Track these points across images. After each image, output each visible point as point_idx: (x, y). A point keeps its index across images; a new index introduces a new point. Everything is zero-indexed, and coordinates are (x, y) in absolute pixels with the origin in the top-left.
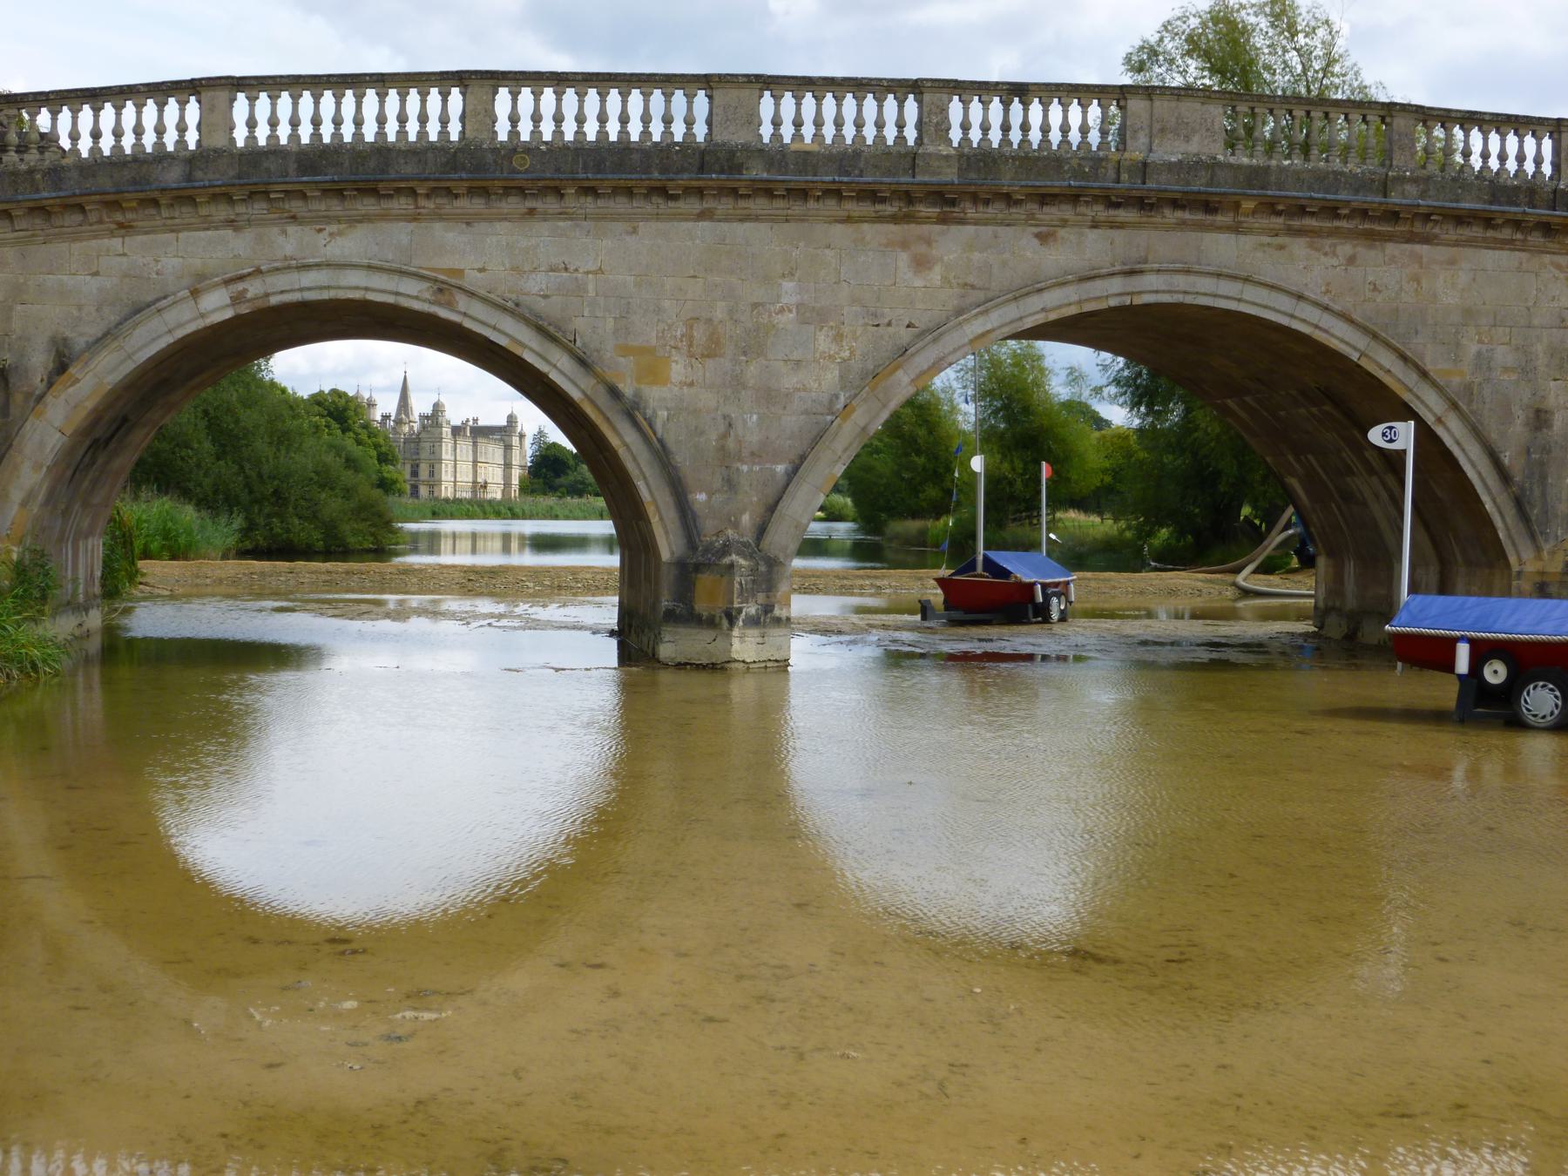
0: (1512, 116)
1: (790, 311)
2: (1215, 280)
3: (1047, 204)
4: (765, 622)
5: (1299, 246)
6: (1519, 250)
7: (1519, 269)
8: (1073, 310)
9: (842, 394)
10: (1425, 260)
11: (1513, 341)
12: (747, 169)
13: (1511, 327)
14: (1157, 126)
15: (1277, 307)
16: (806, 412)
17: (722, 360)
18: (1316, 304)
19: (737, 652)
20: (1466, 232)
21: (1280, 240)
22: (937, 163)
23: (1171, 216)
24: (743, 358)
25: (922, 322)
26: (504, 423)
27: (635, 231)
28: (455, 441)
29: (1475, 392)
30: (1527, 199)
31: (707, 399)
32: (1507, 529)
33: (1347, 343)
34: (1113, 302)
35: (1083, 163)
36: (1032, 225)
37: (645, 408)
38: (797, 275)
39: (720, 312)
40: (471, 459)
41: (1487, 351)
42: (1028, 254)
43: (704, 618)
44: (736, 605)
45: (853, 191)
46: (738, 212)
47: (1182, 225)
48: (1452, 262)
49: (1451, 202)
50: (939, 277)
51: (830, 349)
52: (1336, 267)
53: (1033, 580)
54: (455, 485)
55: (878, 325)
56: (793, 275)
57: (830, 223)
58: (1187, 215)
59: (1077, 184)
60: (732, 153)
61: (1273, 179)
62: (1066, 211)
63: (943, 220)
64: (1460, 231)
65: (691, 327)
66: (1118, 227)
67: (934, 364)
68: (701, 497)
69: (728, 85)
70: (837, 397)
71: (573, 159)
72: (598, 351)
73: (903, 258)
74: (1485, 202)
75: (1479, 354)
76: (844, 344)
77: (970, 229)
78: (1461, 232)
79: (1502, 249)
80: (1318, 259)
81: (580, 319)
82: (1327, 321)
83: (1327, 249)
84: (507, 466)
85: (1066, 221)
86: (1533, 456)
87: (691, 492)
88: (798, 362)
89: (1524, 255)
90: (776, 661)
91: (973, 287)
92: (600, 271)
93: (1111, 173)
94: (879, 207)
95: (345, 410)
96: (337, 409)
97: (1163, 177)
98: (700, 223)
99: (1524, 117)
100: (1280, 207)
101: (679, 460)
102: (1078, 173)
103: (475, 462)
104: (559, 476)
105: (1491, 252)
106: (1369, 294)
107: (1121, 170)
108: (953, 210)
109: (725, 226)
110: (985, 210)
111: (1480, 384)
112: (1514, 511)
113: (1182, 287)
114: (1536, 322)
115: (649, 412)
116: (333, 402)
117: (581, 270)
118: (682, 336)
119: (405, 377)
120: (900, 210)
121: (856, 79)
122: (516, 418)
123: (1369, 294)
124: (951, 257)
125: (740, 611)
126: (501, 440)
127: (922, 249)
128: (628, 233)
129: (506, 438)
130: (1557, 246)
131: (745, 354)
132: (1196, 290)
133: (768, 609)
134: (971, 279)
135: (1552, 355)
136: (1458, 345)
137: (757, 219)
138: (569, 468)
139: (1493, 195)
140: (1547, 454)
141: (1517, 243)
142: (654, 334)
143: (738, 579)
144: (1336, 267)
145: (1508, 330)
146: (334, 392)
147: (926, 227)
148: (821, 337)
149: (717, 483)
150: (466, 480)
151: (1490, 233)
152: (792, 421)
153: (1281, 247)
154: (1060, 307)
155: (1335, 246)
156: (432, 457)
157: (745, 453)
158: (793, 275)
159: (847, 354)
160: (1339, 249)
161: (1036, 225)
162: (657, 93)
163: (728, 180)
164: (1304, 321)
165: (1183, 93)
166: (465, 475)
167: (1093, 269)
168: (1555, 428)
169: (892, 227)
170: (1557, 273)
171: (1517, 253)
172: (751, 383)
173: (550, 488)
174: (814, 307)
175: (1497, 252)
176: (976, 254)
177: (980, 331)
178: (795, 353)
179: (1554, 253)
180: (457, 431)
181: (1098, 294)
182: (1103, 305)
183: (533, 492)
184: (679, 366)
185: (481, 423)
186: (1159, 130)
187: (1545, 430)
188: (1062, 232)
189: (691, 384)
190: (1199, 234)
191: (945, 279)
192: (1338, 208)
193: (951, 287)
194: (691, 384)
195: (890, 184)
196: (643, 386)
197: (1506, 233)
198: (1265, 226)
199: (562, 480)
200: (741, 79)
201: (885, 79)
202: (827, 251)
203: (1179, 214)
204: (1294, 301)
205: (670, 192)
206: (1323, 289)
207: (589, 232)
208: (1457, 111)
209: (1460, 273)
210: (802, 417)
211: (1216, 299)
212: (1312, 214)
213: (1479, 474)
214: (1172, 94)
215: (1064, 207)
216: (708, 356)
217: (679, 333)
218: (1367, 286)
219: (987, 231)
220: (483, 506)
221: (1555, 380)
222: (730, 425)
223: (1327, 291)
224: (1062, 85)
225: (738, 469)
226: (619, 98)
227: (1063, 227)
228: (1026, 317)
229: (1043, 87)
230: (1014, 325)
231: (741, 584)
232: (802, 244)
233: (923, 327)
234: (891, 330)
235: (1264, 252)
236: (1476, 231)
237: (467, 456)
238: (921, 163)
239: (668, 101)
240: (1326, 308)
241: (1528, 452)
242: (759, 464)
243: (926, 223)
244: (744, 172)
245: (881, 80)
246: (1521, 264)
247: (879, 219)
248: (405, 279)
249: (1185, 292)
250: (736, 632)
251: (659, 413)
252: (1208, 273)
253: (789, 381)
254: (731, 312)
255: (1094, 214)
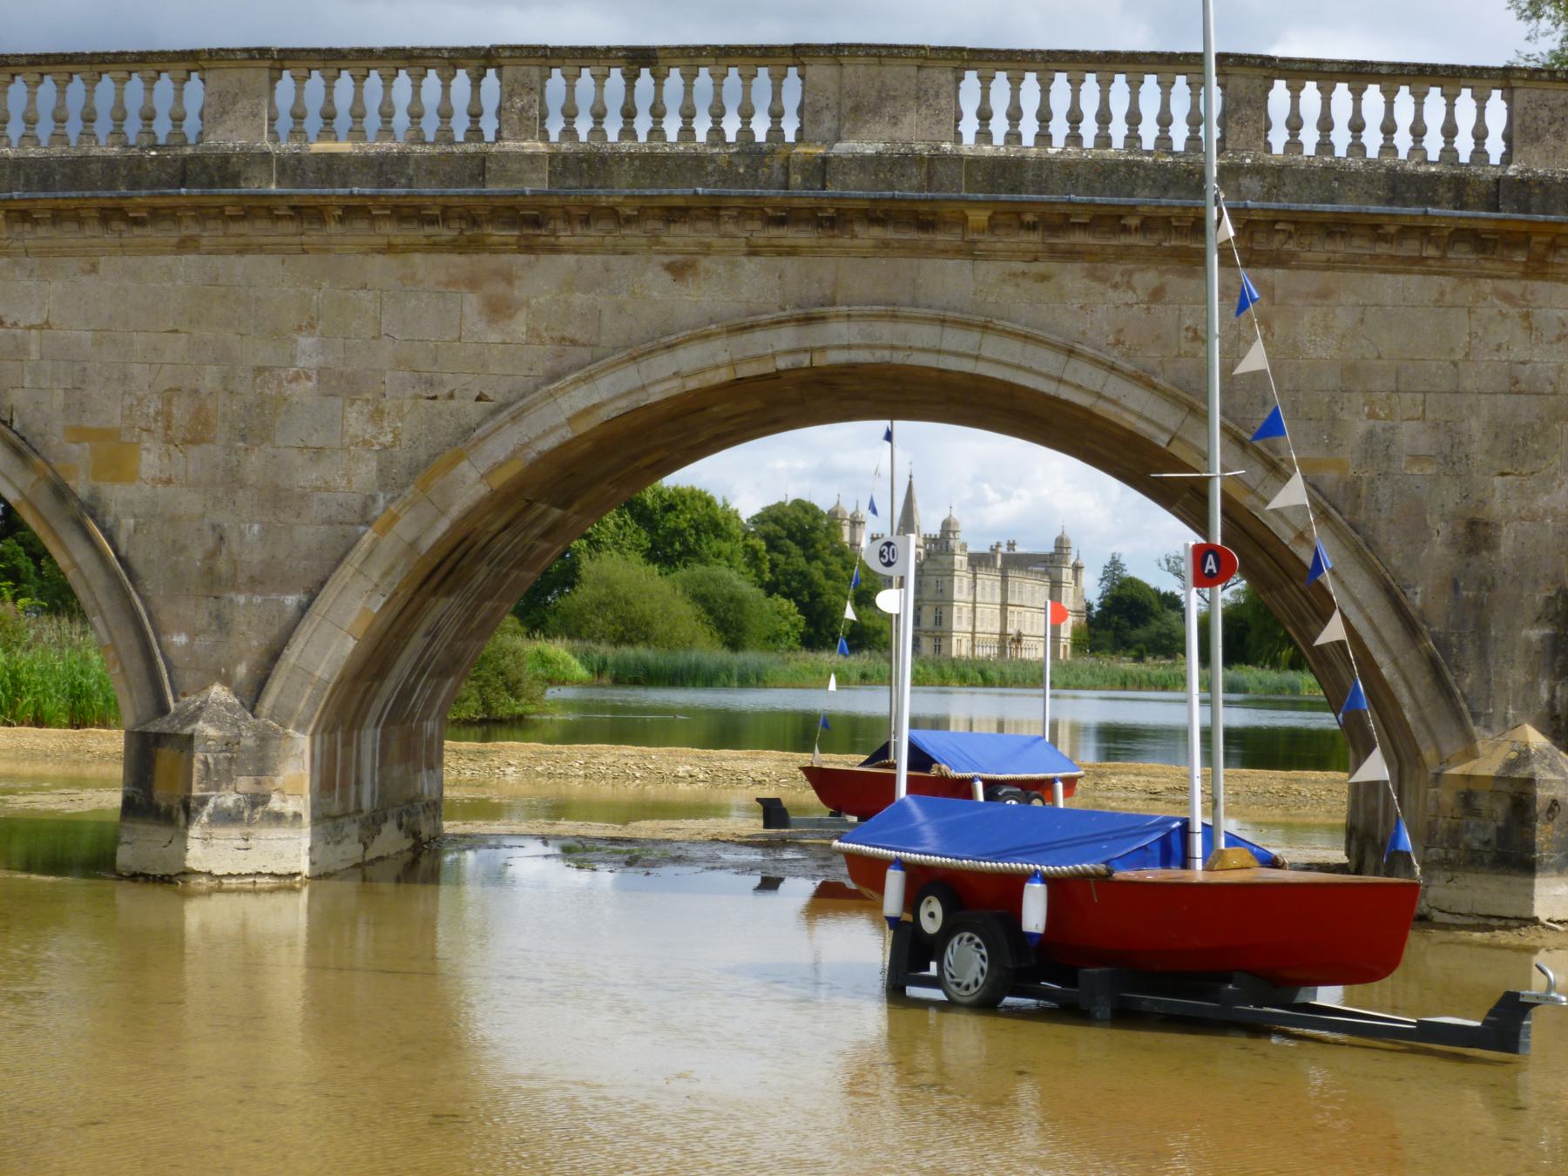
0: (1425, 66)
1: (309, 378)
2: (938, 328)
3: (675, 222)
4: (251, 817)
5: (1072, 277)
6: (1439, 274)
7: (1439, 302)
8: (723, 376)
9: (382, 495)
10: (1278, 291)
11: (1429, 415)
12: (246, 179)
13: (1424, 393)
14: (849, 103)
15: (1035, 367)
16: (329, 522)
17: (211, 447)
18: (1096, 362)
19: (196, 859)
20: (1340, 248)
21: (1040, 267)
22: (516, 167)
23: (869, 235)
24: (241, 444)
25: (497, 396)
26: (987, 550)
27: (94, 269)
28: (975, 575)
29: (1364, 492)
30: (1450, 195)
31: (189, 502)
32: (1419, 707)
33: (1148, 420)
34: (782, 363)
35: (736, 160)
36: (659, 253)
37: (104, 515)
38: (319, 328)
39: (209, 379)
40: (998, 599)
41: (1384, 429)
42: (656, 294)
43: (162, 810)
44: (196, 793)
45: (384, 207)
46: (233, 240)
47: (884, 246)
48: (1324, 294)
49: (1322, 202)
50: (524, 329)
51: (365, 430)
52: (1131, 305)
53: (969, 775)
54: (973, 639)
55: (434, 398)
56: (313, 327)
57: (366, 253)
58: (889, 234)
59: (707, 191)
60: (225, 158)
61: (1029, 176)
62: (706, 233)
63: (528, 248)
64: (1329, 246)
65: (169, 401)
66: (789, 254)
67: (514, 452)
68: (180, 639)
69: (224, 64)
70: (374, 499)
71: (12, 173)
72: (42, 435)
73: (472, 302)
74: (1379, 200)
75: (1371, 434)
76: (385, 424)
77: (569, 260)
78: (1332, 248)
79: (1409, 272)
80: (1103, 294)
81: (19, 392)
82: (1114, 386)
83: (1118, 278)
84: (1059, 615)
85: (708, 246)
86: (1465, 593)
87: (165, 633)
88: (319, 450)
89: (1447, 282)
90: (272, 875)
91: (574, 342)
92: (47, 325)
93: (778, 175)
94: (429, 230)
95: (813, 529)
96: (801, 528)
97: (853, 178)
98: (183, 258)
99: (1447, 67)
100: (1029, 218)
101: (149, 587)
102: (727, 174)
103: (1004, 605)
104: (1137, 627)
105: (1389, 277)
106: (1185, 346)
107: (791, 169)
108: (538, 232)
109: (217, 260)
110: (585, 232)
111: (1372, 481)
112: (1428, 679)
113: (886, 340)
114: (1468, 384)
115: (110, 520)
116: (796, 519)
117: (21, 325)
118: (157, 413)
119: (910, 483)
120: (461, 233)
121: (403, 50)
122: (1068, 542)
123: (1185, 346)
124: (542, 300)
125: (203, 801)
126: (1047, 573)
127: (499, 288)
128: (84, 272)
129: (1051, 570)
130: (1501, 266)
131: (243, 438)
132: (909, 344)
133: (258, 800)
134: (571, 331)
135: (1497, 436)
136: (1334, 420)
137: (261, 249)
138: (1152, 614)
139: (1393, 189)
140: (1489, 590)
141: (1430, 262)
142: (119, 411)
143: (199, 756)
144: (1131, 305)
145: (1420, 397)
146: (799, 504)
147: (505, 258)
148: (352, 415)
149: (202, 619)
150: (990, 629)
151: (1382, 249)
152: (308, 534)
153: (1044, 278)
154: (702, 371)
155: (1130, 273)
156: (939, 596)
157: (242, 578)
158: (313, 327)
159: (390, 437)
160: (1137, 279)
161: (666, 253)
162: (1001, 77)
163: (202, 195)
164: (1079, 387)
165: (884, 53)
166: (989, 623)
167: (753, 315)
168: (1502, 550)
169: (456, 259)
170: (1505, 308)
171: (1435, 277)
172: (252, 478)
173: (1121, 645)
174: (342, 373)
175: (1401, 278)
176: (578, 294)
177: (582, 404)
178: (314, 437)
179: (1499, 277)
180: (978, 561)
181: (760, 351)
182: (768, 368)
183: (1095, 648)
184: (151, 456)
185: (1019, 550)
186: (858, 111)
187: (1484, 553)
188: (704, 263)
189: (169, 481)
190: (915, 262)
191: (533, 332)
192: (1121, 217)
193: (542, 343)
194: (169, 481)
195: (434, 196)
196: (101, 484)
197: (1410, 248)
198: (1014, 246)
199: (1140, 633)
200: (239, 56)
201: (446, 49)
202: (362, 294)
203: (877, 232)
204: (1062, 358)
205: (131, 215)
206: (1111, 339)
207: (32, 271)
208: (1332, 62)
209: (1338, 311)
210: (324, 528)
211: (942, 358)
212: (1084, 227)
213: (1370, 620)
214: (867, 55)
215: (701, 225)
216: (193, 442)
217: (152, 411)
218: (1183, 333)
219: (593, 263)
220: (940, 667)
221: (1503, 474)
222: (221, 538)
223: (1118, 342)
224: (704, 48)
225: (231, 601)
226: (1127, 88)
227: (706, 254)
228: (650, 385)
229: (677, 52)
230: (634, 397)
231: (206, 763)
232: (326, 284)
233: (499, 399)
234: (453, 404)
235: (1017, 285)
236: (1358, 246)
237: (992, 595)
238: (494, 167)
239: (1357, 100)
240: (1112, 368)
241: (1455, 586)
242: (261, 594)
243: (504, 252)
244: (243, 184)
245: (439, 50)
246: (1442, 294)
247: (434, 247)
248: (953, 349)
249: (893, 348)
250: (195, 831)
251: (124, 521)
252: (926, 319)
253: (307, 477)
254: (225, 379)
255: (747, 235)
